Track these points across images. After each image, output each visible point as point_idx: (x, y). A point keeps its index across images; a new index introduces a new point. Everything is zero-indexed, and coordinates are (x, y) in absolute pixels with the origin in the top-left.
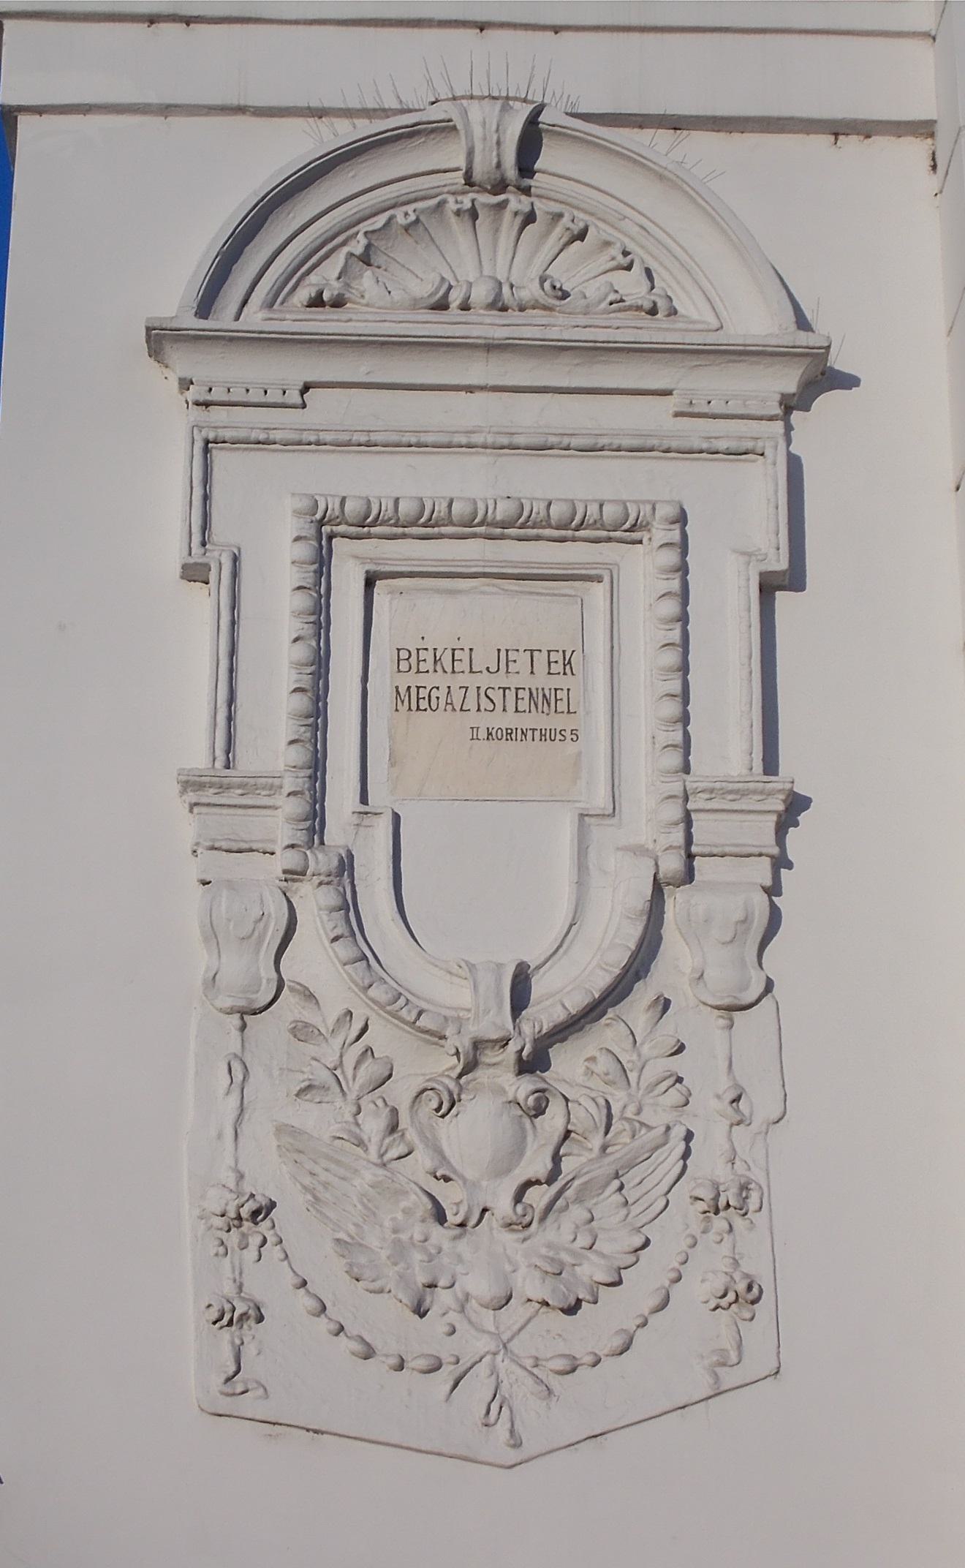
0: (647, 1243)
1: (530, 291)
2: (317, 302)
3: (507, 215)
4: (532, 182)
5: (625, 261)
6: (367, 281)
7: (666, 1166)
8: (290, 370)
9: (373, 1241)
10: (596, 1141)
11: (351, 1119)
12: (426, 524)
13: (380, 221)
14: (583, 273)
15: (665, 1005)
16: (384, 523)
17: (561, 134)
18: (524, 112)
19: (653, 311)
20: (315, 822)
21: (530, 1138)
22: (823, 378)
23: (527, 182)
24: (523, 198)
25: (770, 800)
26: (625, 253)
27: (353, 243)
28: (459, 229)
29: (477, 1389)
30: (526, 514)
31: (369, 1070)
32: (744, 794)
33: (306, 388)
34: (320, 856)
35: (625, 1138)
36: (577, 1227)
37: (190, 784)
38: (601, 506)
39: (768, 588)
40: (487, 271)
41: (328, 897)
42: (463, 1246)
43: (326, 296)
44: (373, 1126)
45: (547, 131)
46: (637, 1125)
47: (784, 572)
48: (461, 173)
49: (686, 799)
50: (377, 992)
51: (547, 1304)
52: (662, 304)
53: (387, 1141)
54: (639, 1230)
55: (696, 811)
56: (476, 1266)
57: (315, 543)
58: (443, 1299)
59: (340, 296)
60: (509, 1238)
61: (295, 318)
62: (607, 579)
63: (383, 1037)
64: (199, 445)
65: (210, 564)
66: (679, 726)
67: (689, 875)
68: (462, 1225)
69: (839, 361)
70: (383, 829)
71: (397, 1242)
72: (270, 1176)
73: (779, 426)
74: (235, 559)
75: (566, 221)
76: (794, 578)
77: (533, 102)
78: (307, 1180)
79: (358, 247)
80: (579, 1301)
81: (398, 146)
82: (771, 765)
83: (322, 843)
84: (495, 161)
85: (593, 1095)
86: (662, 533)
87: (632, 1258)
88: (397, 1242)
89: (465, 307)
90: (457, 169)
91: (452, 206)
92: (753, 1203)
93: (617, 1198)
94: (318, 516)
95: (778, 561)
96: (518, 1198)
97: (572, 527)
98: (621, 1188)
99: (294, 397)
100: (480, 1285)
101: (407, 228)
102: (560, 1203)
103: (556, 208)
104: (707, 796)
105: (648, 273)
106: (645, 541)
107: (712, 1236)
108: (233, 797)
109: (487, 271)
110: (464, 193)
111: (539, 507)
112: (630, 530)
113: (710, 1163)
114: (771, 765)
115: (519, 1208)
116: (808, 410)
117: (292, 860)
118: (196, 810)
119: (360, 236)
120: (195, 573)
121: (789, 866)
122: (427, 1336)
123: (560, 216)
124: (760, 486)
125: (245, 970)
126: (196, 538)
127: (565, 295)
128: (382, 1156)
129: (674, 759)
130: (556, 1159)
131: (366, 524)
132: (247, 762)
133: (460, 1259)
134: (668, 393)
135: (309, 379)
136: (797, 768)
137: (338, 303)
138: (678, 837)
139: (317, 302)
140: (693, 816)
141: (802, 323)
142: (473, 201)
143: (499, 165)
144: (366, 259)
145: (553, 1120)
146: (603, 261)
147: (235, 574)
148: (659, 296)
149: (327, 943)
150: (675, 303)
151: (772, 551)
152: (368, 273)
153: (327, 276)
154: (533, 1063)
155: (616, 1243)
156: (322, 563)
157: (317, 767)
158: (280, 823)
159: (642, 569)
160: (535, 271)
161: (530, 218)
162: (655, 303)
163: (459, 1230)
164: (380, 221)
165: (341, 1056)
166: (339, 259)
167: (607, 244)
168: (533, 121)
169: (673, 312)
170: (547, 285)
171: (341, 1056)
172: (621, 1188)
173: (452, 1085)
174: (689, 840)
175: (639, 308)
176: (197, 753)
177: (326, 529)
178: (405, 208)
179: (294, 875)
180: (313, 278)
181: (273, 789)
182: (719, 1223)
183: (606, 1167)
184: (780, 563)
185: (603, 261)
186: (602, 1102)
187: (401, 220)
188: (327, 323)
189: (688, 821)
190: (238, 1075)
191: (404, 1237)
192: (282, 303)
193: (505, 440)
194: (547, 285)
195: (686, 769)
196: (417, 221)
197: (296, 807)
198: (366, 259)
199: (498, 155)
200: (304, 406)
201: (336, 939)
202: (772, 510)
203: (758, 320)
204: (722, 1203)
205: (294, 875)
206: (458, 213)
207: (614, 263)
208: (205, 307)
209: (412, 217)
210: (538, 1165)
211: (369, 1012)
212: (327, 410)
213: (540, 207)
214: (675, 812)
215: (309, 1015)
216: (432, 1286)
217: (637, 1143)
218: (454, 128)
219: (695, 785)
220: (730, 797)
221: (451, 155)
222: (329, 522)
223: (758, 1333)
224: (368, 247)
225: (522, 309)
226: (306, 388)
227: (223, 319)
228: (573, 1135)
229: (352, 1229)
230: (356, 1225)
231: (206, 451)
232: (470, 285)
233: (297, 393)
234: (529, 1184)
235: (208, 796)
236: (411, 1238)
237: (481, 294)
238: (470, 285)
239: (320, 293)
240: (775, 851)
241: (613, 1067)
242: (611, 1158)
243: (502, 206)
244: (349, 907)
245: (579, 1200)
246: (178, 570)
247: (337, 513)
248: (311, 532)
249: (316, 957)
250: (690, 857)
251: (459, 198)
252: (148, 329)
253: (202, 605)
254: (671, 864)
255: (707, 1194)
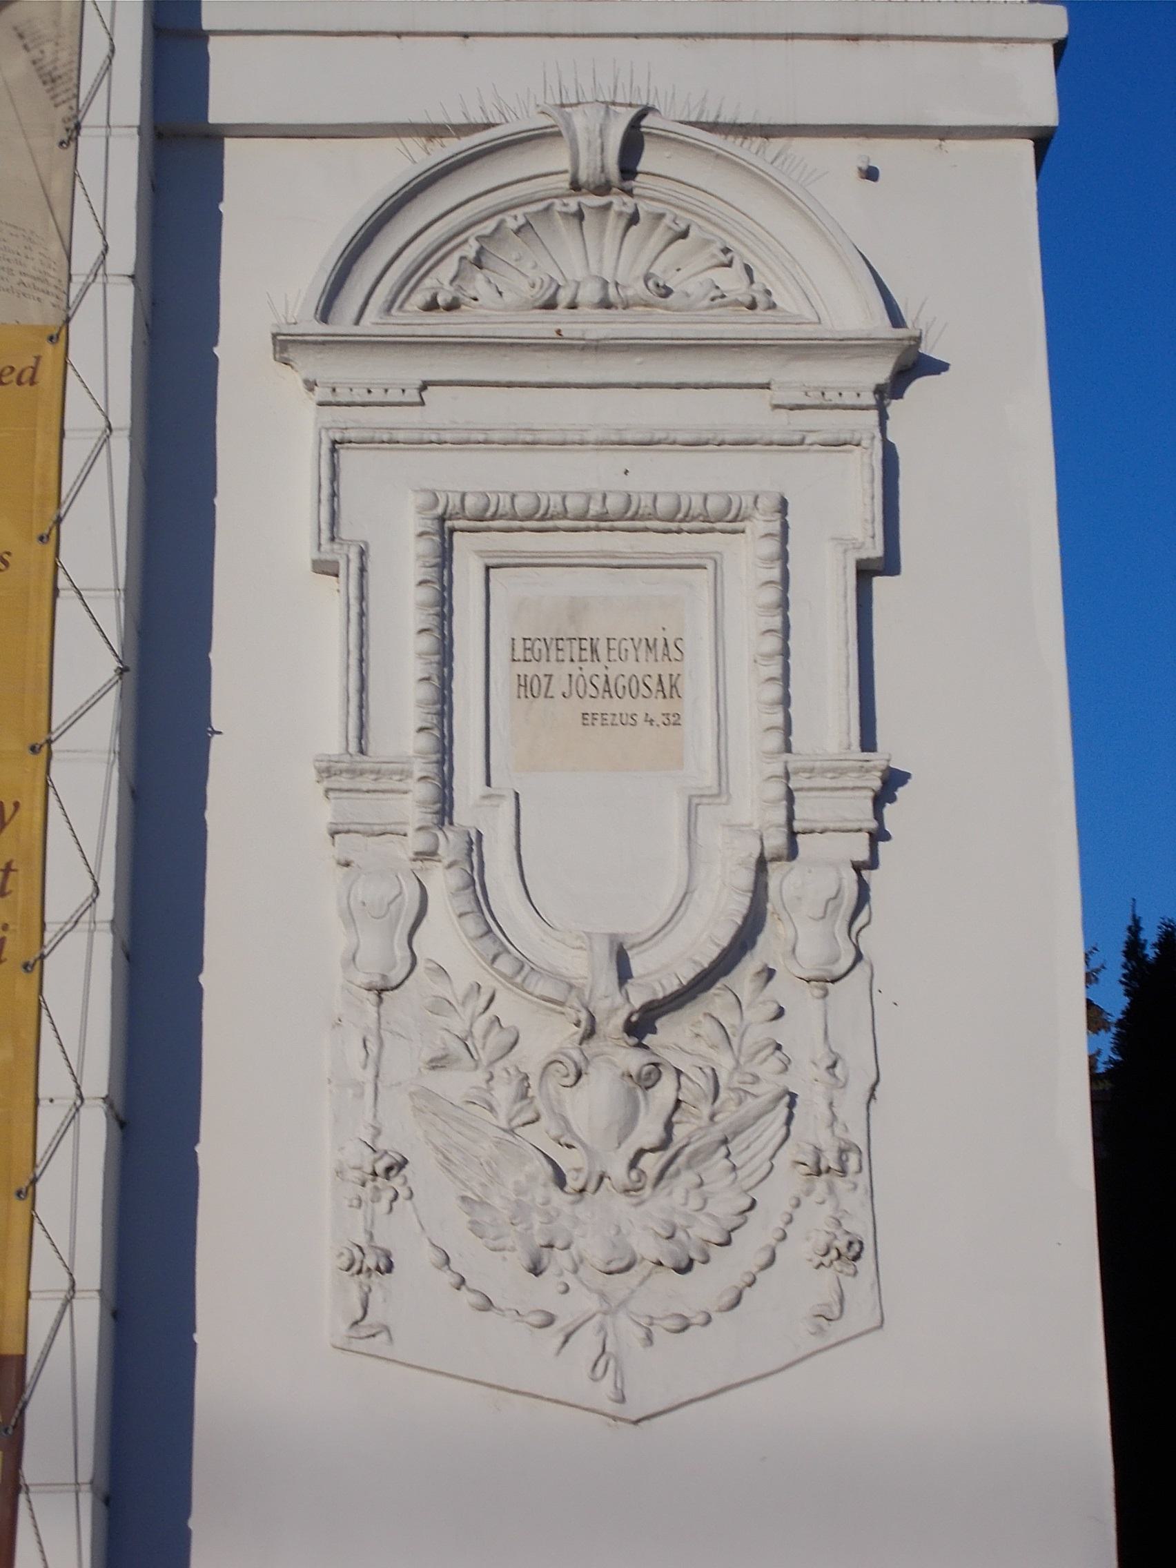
0: (754, 1203)
1: (637, 289)
2: (432, 306)
3: (612, 214)
4: (633, 183)
5: (725, 259)
6: (479, 284)
7: (756, 1161)
8: (407, 371)
9: (497, 1202)
10: (706, 1110)
11: (484, 1086)
12: (542, 518)
13: (490, 225)
14: (691, 274)
15: (770, 973)
16: (502, 517)
17: (665, 138)
18: (627, 115)
19: (753, 306)
20: (444, 809)
21: (642, 1115)
22: (913, 366)
23: (627, 184)
24: (626, 198)
25: (868, 776)
26: (726, 251)
27: (466, 247)
28: (565, 231)
29: (586, 1345)
30: (633, 509)
31: (498, 1039)
32: (843, 772)
33: (424, 386)
34: (450, 835)
35: (732, 1106)
36: (687, 1192)
37: (327, 771)
38: (705, 499)
39: (865, 573)
40: (594, 269)
41: (455, 878)
42: (582, 1210)
43: (440, 300)
44: (503, 1093)
45: (648, 134)
46: (742, 1094)
47: (879, 559)
48: (567, 177)
49: (787, 776)
50: (505, 964)
51: (660, 1264)
52: (760, 298)
53: (518, 1106)
54: (746, 1192)
55: (801, 789)
56: (594, 1228)
57: (437, 539)
58: (562, 1259)
59: (455, 299)
60: (623, 1200)
61: (412, 320)
62: (710, 566)
63: (509, 1007)
64: (326, 447)
65: (343, 560)
66: (780, 709)
67: (792, 852)
68: (582, 1190)
69: (931, 349)
70: (508, 807)
71: (518, 1203)
72: (403, 1135)
73: (873, 416)
74: (362, 553)
75: (667, 221)
76: (890, 564)
77: (637, 106)
78: (439, 1141)
79: (471, 250)
80: (691, 1261)
81: (519, 148)
82: (868, 742)
83: (451, 823)
84: (599, 164)
85: (701, 1063)
86: (762, 523)
87: (739, 1220)
88: (518, 1203)
89: (573, 306)
90: (565, 172)
91: (558, 205)
92: (852, 1164)
93: (726, 1162)
94: (440, 510)
95: (874, 548)
96: (633, 1165)
97: (679, 519)
98: (728, 1155)
99: (412, 395)
100: (595, 1249)
101: (518, 231)
102: (672, 1169)
103: (658, 207)
104: (807, 775)
105: (748, 270)
106: (747, 531)
107: (815, 1197)
108: (366, 782)
109: (594, 269)
110: (569, 196)
111: (647, 501)
112: (729, 519)
113: (812, 1128)
114: (868, 742)
115: (634, 1175)
116: (901, 397)
117: (419, 842)
118: (331, 795)
119: (473, 242)
120: (325, 568)
121: (886, 837)
122: (544, 1292)
123: (661, 216)
124: (858, 475)
125: (379, 952)
126: (325, 534)
127: (667, 292)
128: (510, 1120)
129: (775, 740)
130: (669, 1126)
131: (484, 519)
132: (380, 745)
133: (576, 1221)
134: (766, 386)
135: (425, 378)
136: (894, 748)
137: (453, 306)
138: (780, 815)
139: (432, 306)
140: (795, 794)
141: (896, 319)
142: (579, 204)
143: (603, 168)
144: (478, 263)
145: (665, 1091)
146: (702, 260)
147: (362, 570)
148: (758, 292)
149: (454, 918)
150: (775, 298)
151: (869, 540)
152: (480, 276)
153: (441, 280)
154: (640, 1027)
155: (726, 1204)
156: (445, 557)
157: (445, 751)
158: (411, 805)
159: (746, 555)
160: (640, 270)
161: (634, 219)
162: (754, 299)
163: (578, 1196)
164: (490, 225)
165: (471, 1026)
166: (450, 267)
167: (707, 243)
168: (635, 125)
169: (773, 306)
170: (651, 284)
171: (471, 1026)
172: (728, 1155)
173: (576, 1055)
174: (791, 818)
175: (737, 303)
176: (332, 738)
177: (448, 524)
178: (513, 212)
179: (427, 855)
180: (428, 282)
181: (405, 774)
182: (821, 1183)
183: (716, 1133)
184: (875, 550)
185: (702, 260)
186: (708, 1071)
187: (512, 224)
188: (441, 324)
189: (790, 797)
190: (373, 1047)
191: (526, 1199)
192: (401, 307)
193: (614, 437)
194: (651, 284)
195: (788, 748)
196: (528, 223)
197: (425, 791)
198: (478, 263)
199: (602, 160)
200: (422, 403)
201: (461, 915)
202: (868, 500)
203: (858, 315)
204: (823, 1167)
205: (427, 855)
206: (565, 215)
207: (715, 261)
208: (325, 312)
209: (521, 221)
210: (648, 1131)
211: (495, 984)
212: (444, 408)
213: (644, 207)
214: (777, 790)
215: (441, 989)
216: (551, 1246)
217: (742, 1111)
218: (559, 134)
219: (799, 764)
220: (830, 775)
221: (556, 159)
222: (450, 519)
223: (859, 1288)
224: (480, 252)
225: (626, 307)
226: (424, 386)
227: (343, 323)
228: (683, 1105)
229: (478, 1190)
230: (483, 1185)
231: (333, 451)
232: (578, 284)
233: (416, 392)
234: (641, 1153)
235: (344, 781)
236: (533, 1200)
237: (589, 293)
238: (578, 284)
239: (434, 298)
240: (873, 825)
241: (718, 1035)
242: (717, 1127)
243: (607, 207)
244: (475, 886)
245: (689, 1165)
246: (309, 566)
247: (457, 510)
248: (432, 526)
249: (446, 937)
250: (792, 834)
251: (565, 201)
252: (274, 336)
253: (330, 599)
254: (776, 841)
255: (810, 1159)
